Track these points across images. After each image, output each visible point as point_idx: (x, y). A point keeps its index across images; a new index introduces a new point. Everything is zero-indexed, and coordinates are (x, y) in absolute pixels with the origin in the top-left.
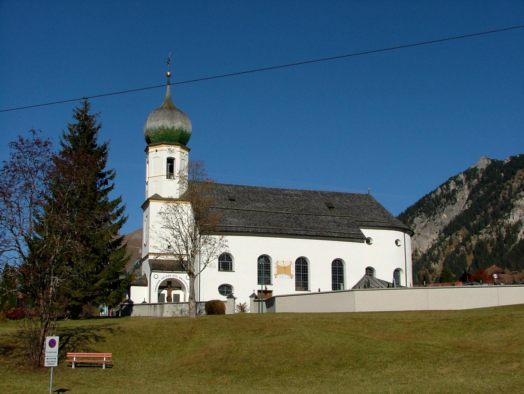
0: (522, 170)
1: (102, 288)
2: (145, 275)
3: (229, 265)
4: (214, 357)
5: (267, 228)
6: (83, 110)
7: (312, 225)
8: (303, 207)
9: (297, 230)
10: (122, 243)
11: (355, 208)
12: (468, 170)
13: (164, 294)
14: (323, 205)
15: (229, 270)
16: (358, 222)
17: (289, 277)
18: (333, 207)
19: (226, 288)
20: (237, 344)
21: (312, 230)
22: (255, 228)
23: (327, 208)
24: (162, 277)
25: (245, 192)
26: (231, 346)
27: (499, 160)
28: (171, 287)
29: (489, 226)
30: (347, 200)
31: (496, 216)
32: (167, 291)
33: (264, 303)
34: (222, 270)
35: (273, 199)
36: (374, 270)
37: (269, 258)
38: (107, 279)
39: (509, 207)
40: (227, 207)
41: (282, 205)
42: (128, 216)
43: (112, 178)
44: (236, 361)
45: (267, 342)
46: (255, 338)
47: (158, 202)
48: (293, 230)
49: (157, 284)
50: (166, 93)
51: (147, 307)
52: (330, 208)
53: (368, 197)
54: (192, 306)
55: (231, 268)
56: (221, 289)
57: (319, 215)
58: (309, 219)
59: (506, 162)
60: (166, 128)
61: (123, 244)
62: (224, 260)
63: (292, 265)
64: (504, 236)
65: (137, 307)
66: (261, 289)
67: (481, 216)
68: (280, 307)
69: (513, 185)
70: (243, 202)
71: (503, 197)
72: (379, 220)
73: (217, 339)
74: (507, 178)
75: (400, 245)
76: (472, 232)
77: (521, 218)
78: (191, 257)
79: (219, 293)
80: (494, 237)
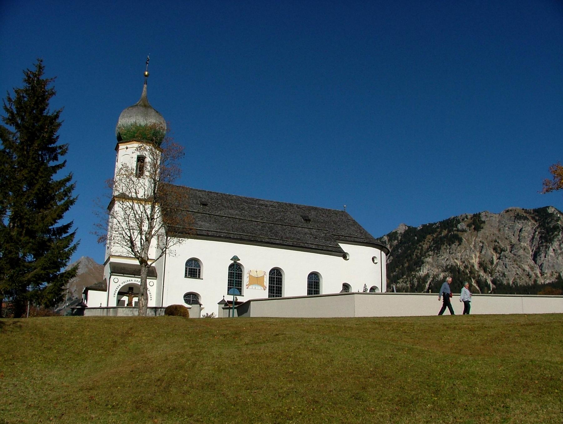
0: (430, 235)
1: (35, 279)
2: (106, 279)
3: (197, 272)
4: (147, 375)
5: (241, 235)
6: (36, 73)
7: (288, 235)
8: (279, 217)
9: (272, 239)
10: (68, 231)
11: (331, 223)
12: (390, 233)
13: (125, 301)
14: (299, 218)
15: (196, 277)
16: (336, 236)
17: (262, 288)
18: (310, 220)
19: (192, 297)
20: (194, 354)
21: (288, 240)
22: (227, 233)
23: (303, 220)
24: (121, 281)
25: (218, 198)
26: (182, 356)
27: (413, 227)
28: (132, 293)
29: (405, 277)
30: (324, 215)
31: (411, 269)
32: (127, 297)
33: (235, 310)
34: (189, 277)
35: (247, 207)
36: (350, 287)
37: (241, 267)
38: (42, 269)
39: (420, 263)
40: (198, 211)
41: (257, 214)
42: (77, 197)
43: (63, 153)
44: (188, 385)
45: (248, 352)
46: (227, 345)
48: (269, 238)
49: (117, 288)
50: (142, 92)
51: (99, 311)
52: (306, 220)
53: (343, 213)
54: (142, 305)
55: (199, 275)
56: (187, 298)
57: (295, 226)
58: (285, 229)
59: (419, 229)
60: (138, 125)
61: (70, 231)
62: (192, 266)
63: (265, 276)
64: (416, 285)
65: (88, 311)
66: (232, 300)
67: (399, 269)
68: (255, 312)
69: (424, 246)
70: (216, 207)
71: (416, 255)
72: (356, 236)
73: (165, 345)
74: (419, 241)
75: (377, 263)
76: (392, 281)
77: (429, 272)
78: (146, 241)
79: (184, 301)
80: (408, 285)
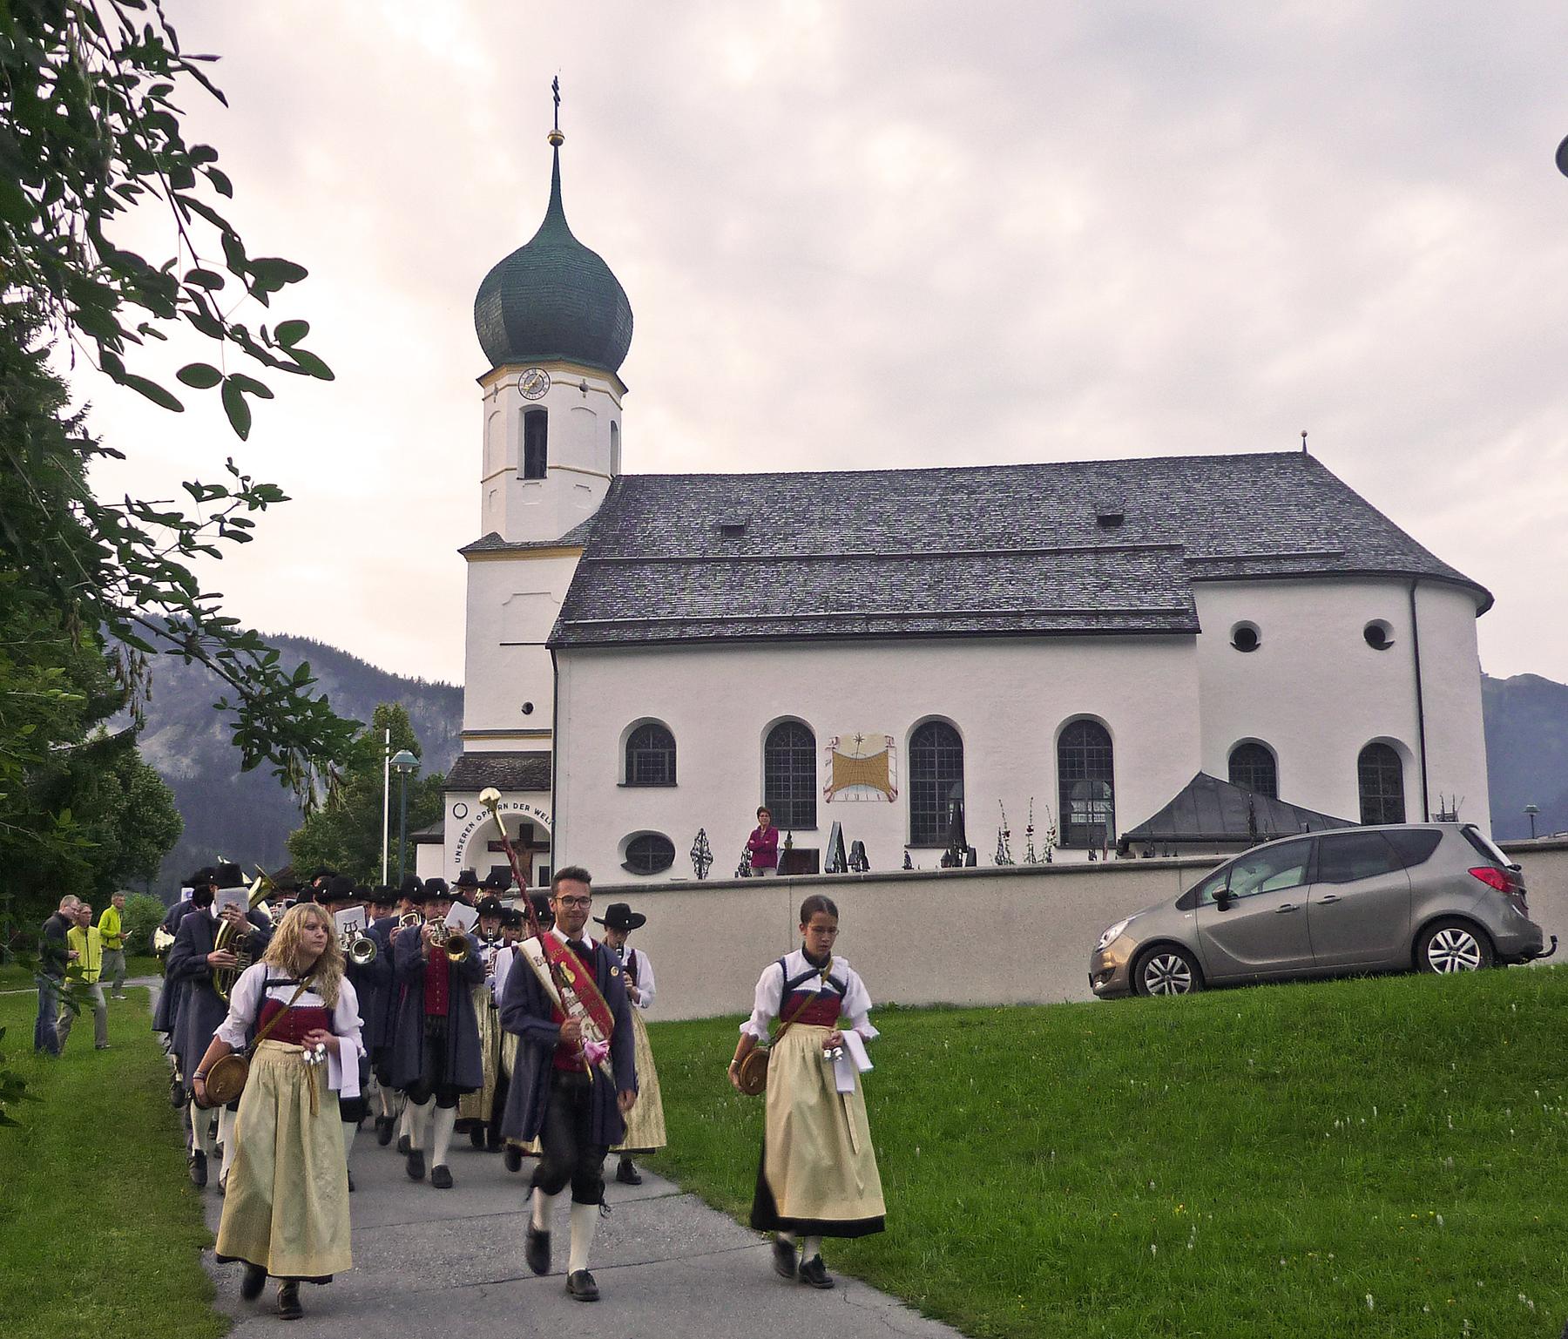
17: (883, 795)
47: (516, 563)
63: (891, 753)
